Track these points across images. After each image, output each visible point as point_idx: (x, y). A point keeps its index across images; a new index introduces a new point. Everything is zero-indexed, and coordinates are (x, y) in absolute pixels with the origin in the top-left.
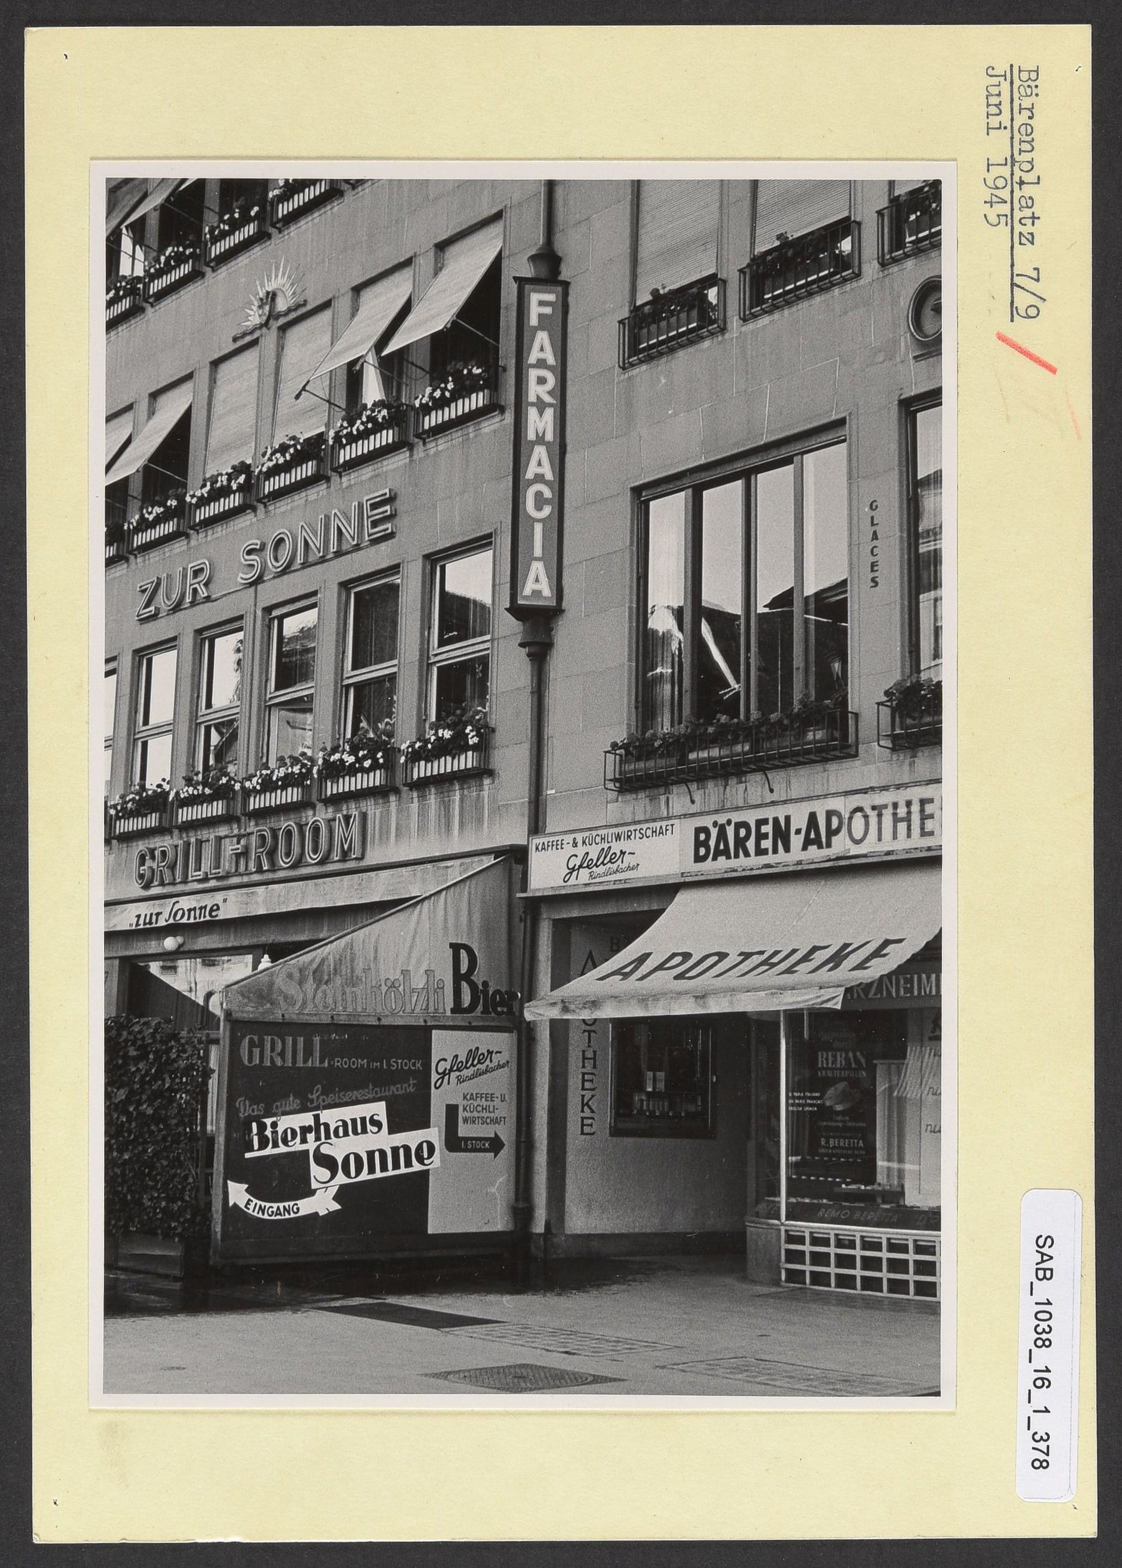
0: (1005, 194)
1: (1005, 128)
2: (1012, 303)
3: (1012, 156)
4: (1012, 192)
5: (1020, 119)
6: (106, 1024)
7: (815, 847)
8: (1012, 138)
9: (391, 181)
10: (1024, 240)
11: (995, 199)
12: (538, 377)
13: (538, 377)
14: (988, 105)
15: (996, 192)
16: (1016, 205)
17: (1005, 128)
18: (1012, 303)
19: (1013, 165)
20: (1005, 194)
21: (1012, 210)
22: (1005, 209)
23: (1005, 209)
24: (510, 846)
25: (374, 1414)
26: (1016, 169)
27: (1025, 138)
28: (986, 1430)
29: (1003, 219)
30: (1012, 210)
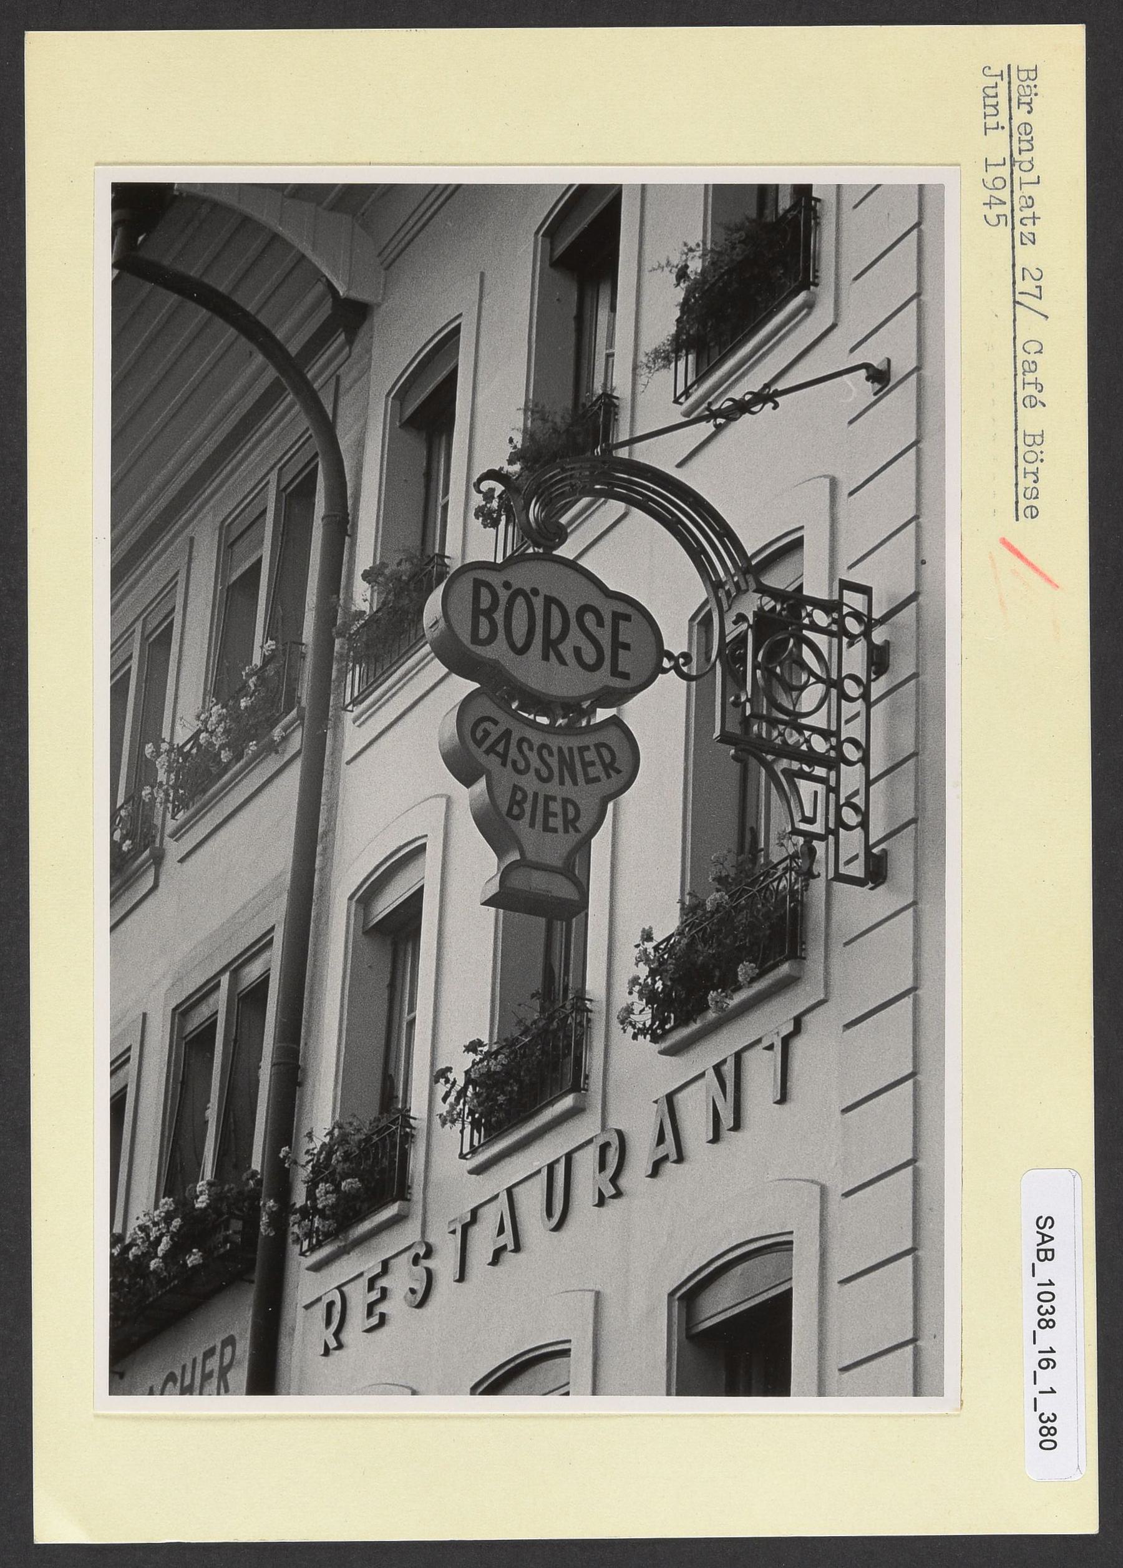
3: (1011, 155)
4: (1012, 192)
5: (1020, 115)
8: (1011, 136)
15: (996, 193)
20: (1005, 195)
21: (1013, 210)
26: (1016, 168)
27: (1024, 137)
29: (1003, 219)
30: (1013, 210)
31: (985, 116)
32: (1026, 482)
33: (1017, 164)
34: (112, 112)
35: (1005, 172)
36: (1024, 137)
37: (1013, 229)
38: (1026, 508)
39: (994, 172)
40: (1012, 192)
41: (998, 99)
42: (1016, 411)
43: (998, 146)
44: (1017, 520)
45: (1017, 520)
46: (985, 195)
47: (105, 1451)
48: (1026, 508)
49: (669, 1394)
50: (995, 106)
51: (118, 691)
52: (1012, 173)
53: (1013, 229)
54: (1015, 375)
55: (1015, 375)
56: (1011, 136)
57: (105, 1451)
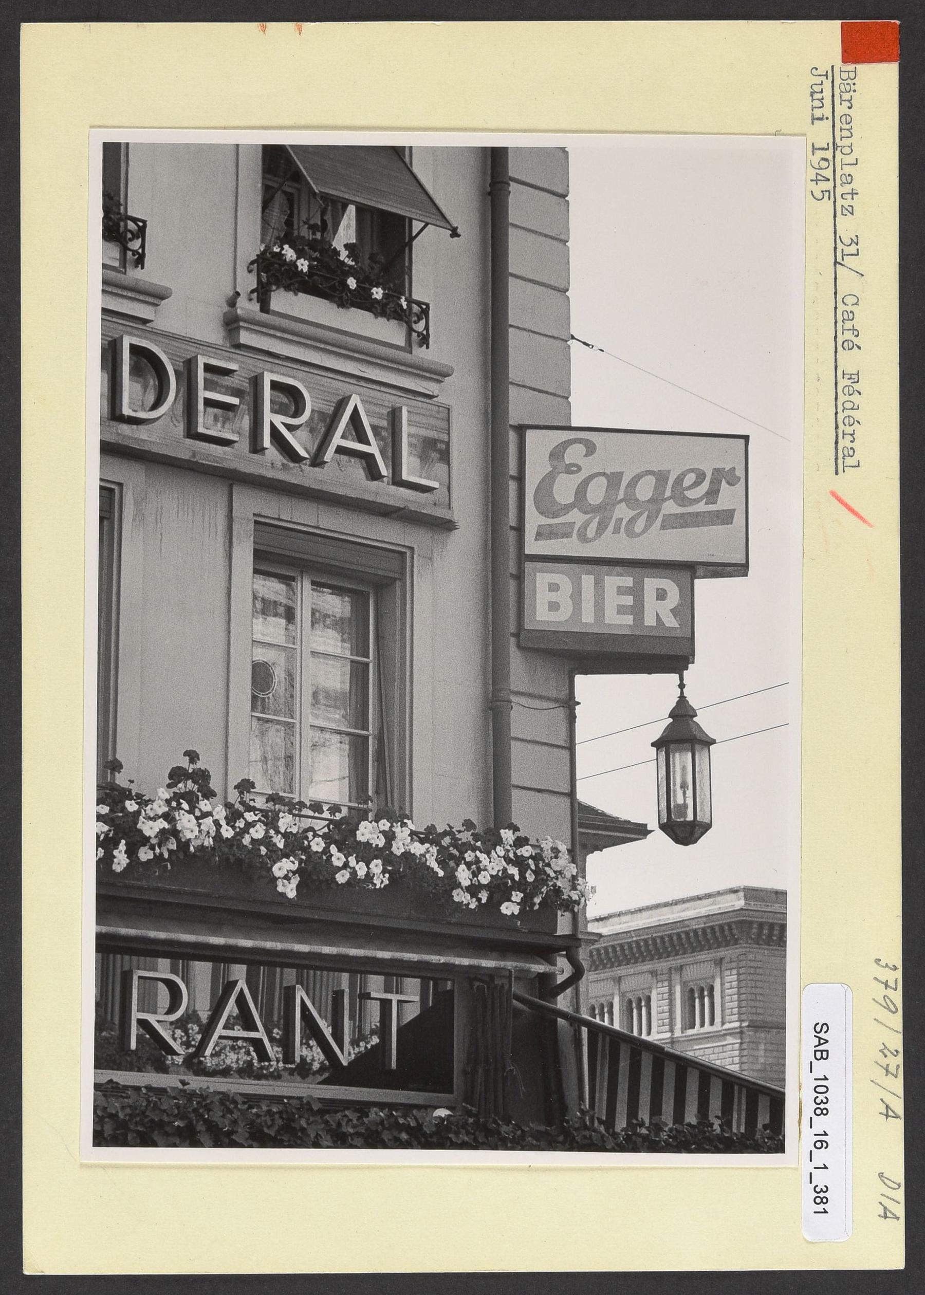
0: (828, 173)
1: (827, 118)
2: (835, 233)
3: (834, 143)
4: (834, 171)
5: (841, 110)
6: (104, 865)
7: (585, 452)
8: (834, 126)
9: (784, 1080)
10: (845, 212)
11: (819, 177)
12: (550, 584)
13: (550, 584)
14: (813, 100)
15: (820, 172)
16: (838, 182)
17: (827, 118)
18: (835, 233)
19: (835, 150)
20: (828, 173)
21: (835, 187)
22: (829, 185)
23: (829, 185)
24: (103, 367)
25: (441, 1168)
26: (838, 153)
27: (845, 126)
28: (824, 1191)
29: (826, 194)
30: (835, 187)
31: (813, 119)
32: (844, 443)
33: (839, 149)
34: (83, 85)
35: (829, 154)
36: (845, 126)
37: (835, 202)
38: (842, 457)
39: (820, 154)
40: (834, 171)
41: (823, 86)
42: (836, 352)
43: (822, 134)
44: (837, 473)
45: (837, 473)
46: (812, 174)
47: (83, 1197)
48: (842, 457)
49: (411, 148)
50: (822, 1057)
51: (99, 616)
52: (834, 157)
53: (835, 202)
54: (836, 322)
55: (836, 322)
56: (834, 126)
57: (83, 1197)
